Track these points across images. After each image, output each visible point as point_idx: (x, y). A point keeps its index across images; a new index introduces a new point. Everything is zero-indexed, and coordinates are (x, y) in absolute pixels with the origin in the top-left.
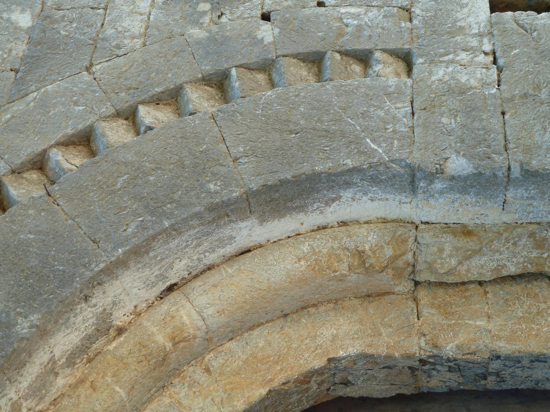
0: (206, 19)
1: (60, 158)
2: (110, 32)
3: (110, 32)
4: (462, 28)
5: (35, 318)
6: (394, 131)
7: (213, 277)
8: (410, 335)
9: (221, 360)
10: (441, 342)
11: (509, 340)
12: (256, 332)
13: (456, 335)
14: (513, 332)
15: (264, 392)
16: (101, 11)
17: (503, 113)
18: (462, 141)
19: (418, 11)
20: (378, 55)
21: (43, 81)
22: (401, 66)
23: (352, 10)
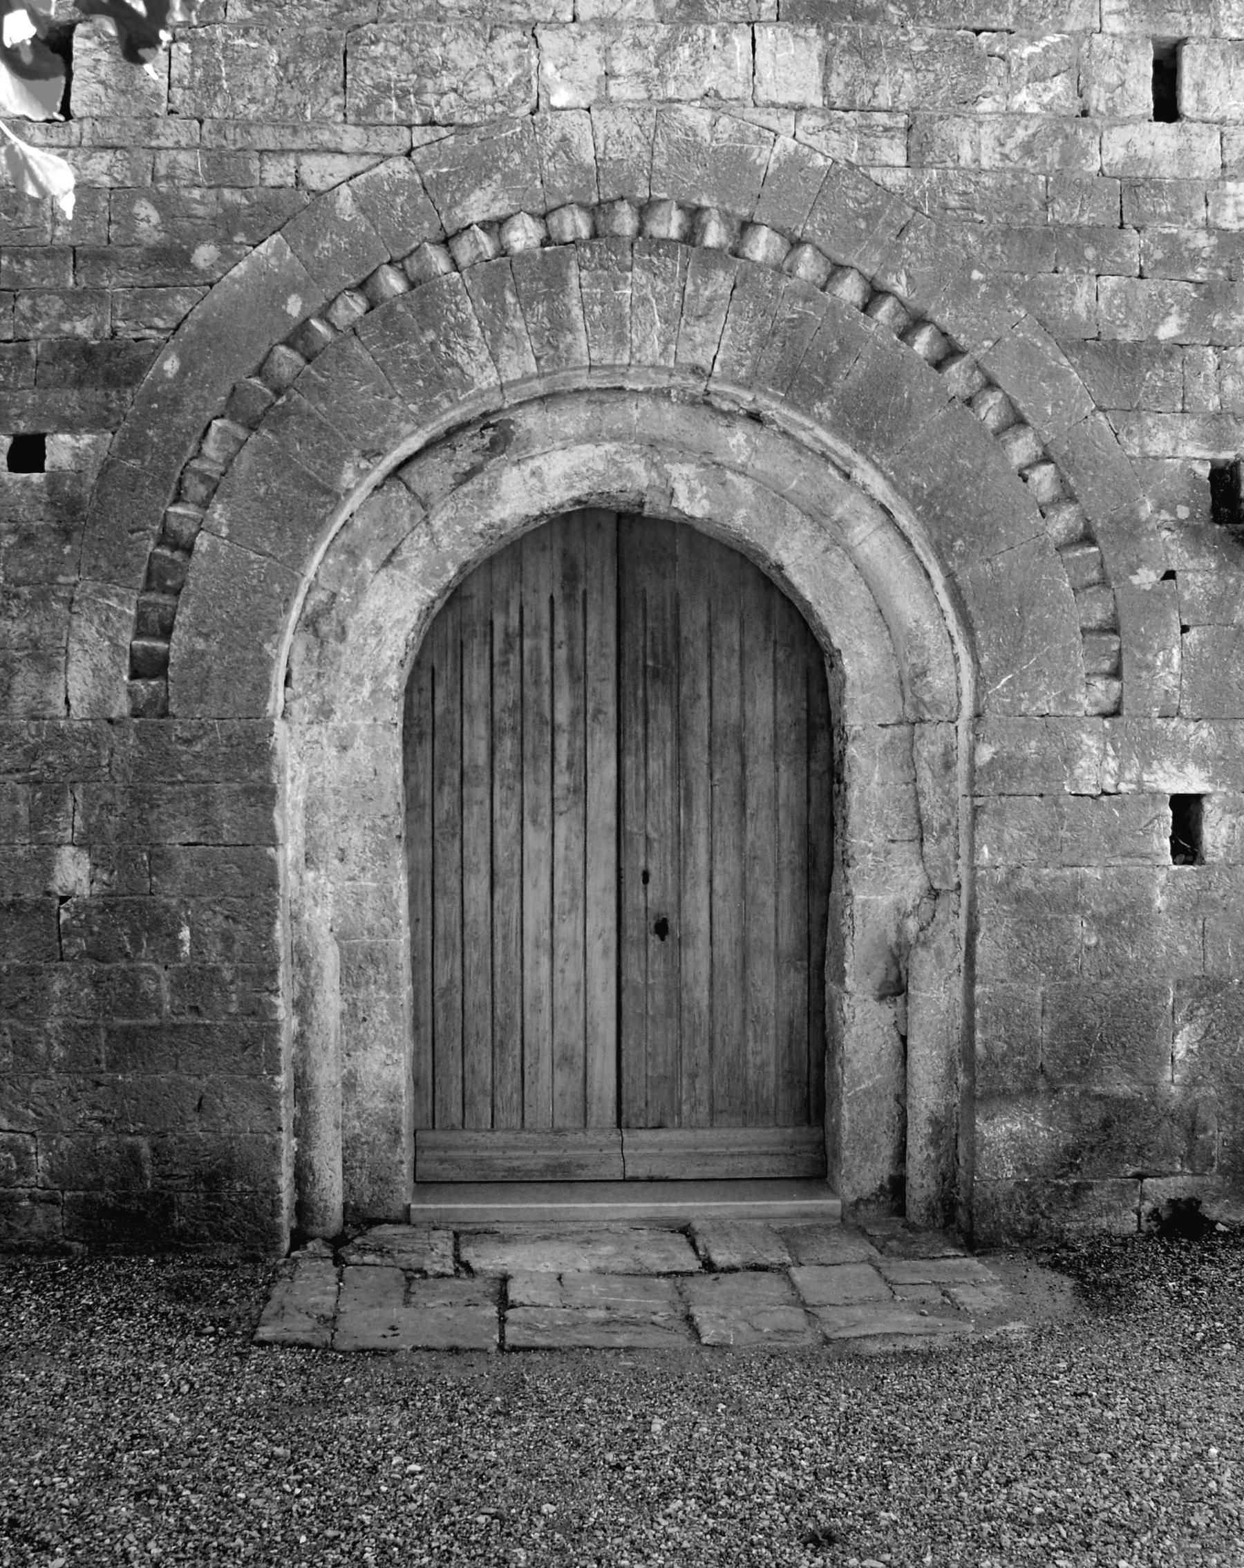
0: (1165, 516)
1: (991, 402)
2: (1150, 422)
3: (1150, 422)
4: (1150, 765)
5: (828, 414)
6: (1021, 700)
7: (897, 549)
8: (864, 717)
9: (836, 560)
10: (857, 743)
11: (861, 801)
12: (864, 588)
13: (864, 756)
14: (868, 804)
15: (809, 598)
16: (1179, 407)
17: (1041, 796)
18: (1009, 758)
19: (1173, 724)
20: (1116, 685)
21: (1082, 367)
22: (1108, 706)
23: (1176, 660)
